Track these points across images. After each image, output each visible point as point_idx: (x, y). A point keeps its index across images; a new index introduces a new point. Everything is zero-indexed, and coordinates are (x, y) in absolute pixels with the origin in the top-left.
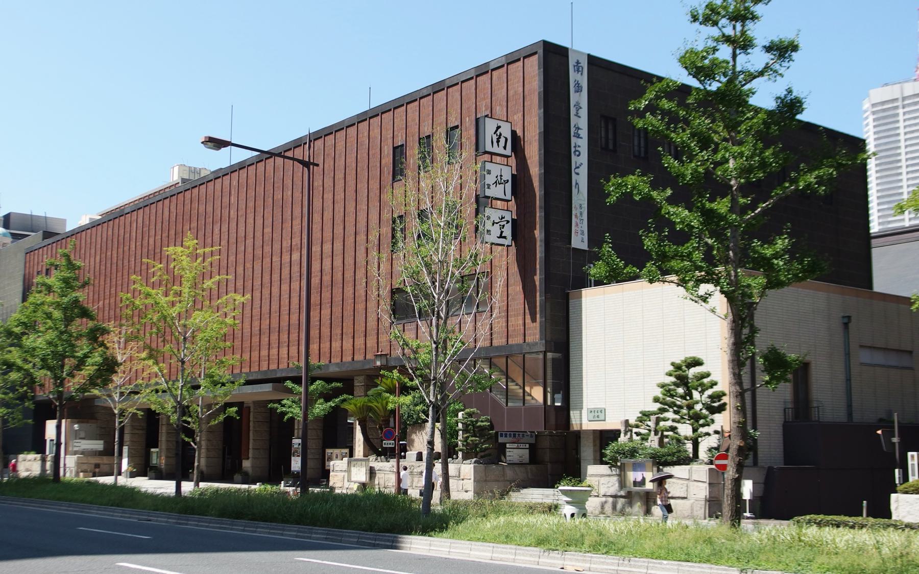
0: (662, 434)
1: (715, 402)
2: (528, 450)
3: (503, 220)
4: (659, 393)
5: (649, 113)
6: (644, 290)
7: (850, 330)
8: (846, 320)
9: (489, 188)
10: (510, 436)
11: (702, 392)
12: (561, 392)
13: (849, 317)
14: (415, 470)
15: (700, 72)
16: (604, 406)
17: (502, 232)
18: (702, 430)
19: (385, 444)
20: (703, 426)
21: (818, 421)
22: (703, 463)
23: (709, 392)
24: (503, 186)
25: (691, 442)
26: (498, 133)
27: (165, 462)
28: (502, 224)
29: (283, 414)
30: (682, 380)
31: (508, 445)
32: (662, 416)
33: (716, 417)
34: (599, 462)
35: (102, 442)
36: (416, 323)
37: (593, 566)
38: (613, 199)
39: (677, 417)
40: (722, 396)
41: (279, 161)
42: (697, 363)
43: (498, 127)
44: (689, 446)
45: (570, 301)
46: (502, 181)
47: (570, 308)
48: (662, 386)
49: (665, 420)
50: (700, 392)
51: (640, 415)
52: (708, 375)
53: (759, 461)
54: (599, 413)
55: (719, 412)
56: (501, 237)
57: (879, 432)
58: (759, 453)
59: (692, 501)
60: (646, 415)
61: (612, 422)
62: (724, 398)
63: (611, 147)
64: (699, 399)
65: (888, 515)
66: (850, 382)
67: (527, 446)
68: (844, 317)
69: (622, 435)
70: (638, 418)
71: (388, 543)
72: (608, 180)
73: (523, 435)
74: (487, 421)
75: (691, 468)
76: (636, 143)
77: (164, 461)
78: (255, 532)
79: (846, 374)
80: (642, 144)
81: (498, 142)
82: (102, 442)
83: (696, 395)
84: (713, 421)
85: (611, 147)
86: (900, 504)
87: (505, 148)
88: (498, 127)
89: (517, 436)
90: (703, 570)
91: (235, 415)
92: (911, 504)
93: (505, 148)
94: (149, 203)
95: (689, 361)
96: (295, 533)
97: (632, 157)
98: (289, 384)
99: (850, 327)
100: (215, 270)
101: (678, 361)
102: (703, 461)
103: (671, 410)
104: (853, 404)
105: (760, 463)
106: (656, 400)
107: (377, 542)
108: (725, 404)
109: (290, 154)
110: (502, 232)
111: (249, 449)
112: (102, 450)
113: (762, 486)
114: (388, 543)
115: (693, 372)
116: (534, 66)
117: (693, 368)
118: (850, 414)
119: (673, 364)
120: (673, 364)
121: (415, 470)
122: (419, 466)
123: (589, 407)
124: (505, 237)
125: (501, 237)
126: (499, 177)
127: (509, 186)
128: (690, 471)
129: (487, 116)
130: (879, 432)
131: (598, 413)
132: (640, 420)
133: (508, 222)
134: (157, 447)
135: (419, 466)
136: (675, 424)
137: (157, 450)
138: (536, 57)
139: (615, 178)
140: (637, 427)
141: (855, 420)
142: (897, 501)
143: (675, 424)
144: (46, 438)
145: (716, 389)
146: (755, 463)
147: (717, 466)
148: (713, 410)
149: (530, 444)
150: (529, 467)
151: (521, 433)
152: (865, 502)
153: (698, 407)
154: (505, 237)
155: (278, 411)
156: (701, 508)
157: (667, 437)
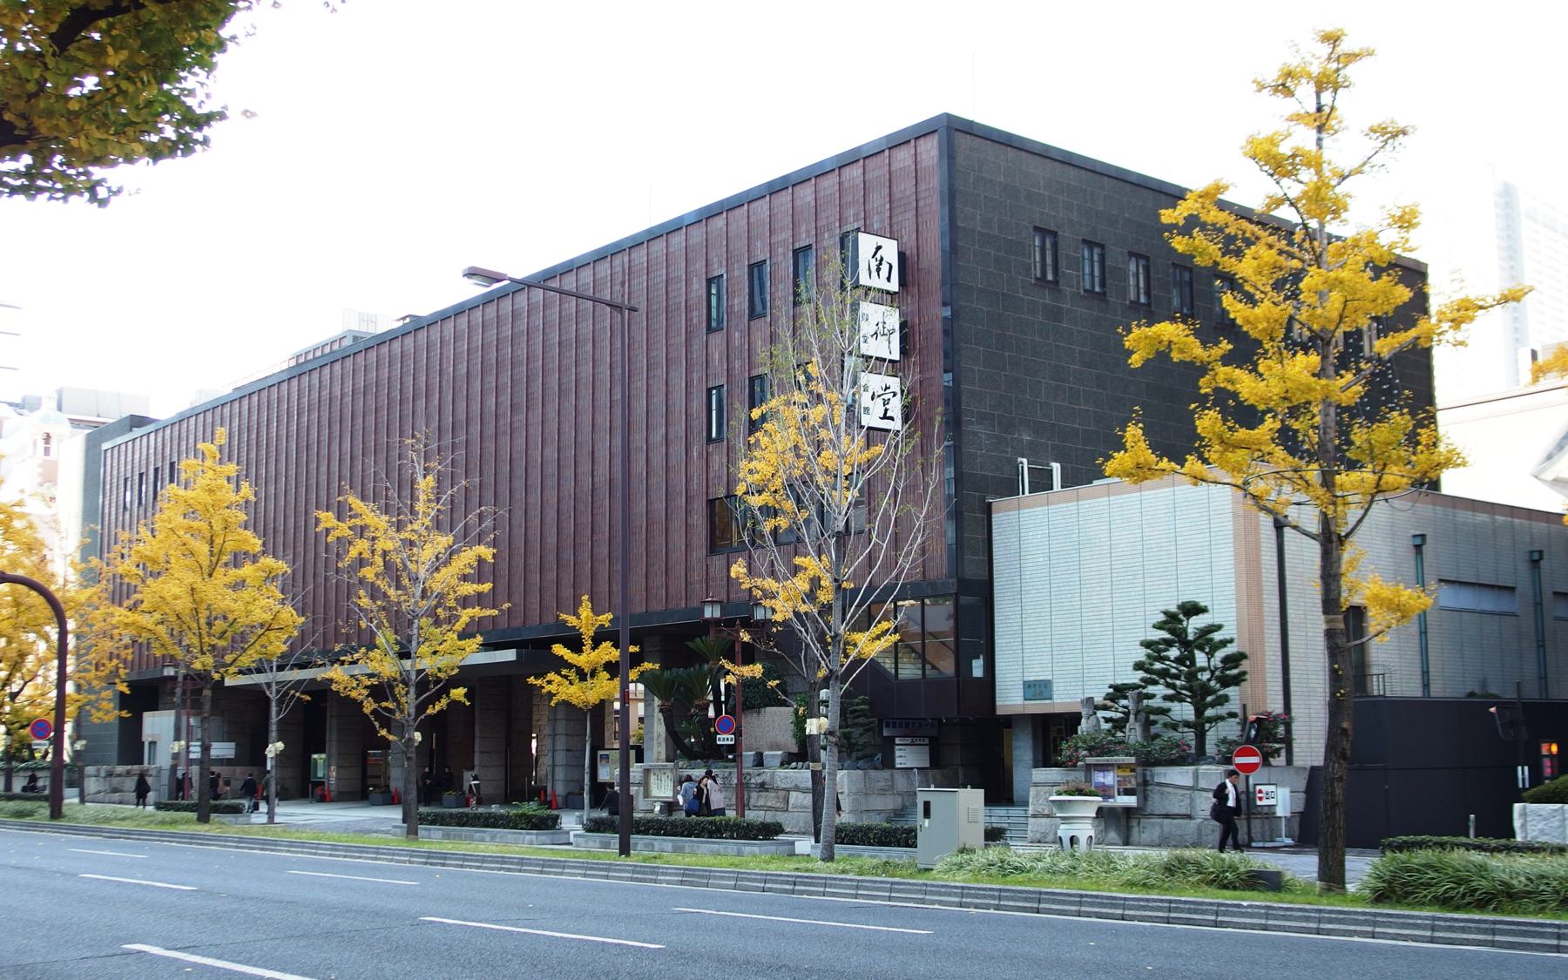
0: (1147, 718)
1: (1230, 669)
2: (927, 748)
3: (888, 391)
4: (1141, 654)
5: (1198, 229)
6: (1111, 498)
7: (1424, 556)
8: (1418, 541)
9: (865, 342)
10: (901, 726)
11: (1210, 655)
12: (981, 657)
13: (1423, 536)
14: (753, 781)
15: (1279, 166)
16: (1050, 678)
17: (886, 410)
18: (1209, 712)
19: (719, 739)
20: (1212, 705)
21: (1384, 696)
22: (1212, 761)
23: (1220, 654)
24: (886, 338)
25: (46, 804)
26: (878, 256)
27: (337, 774)
28: (886, 397)
29: (551, 695)
30: (1179, 637)
31: (897, 741)
32: (1145, 691)
33: (1231, 691)
34: (1041, 764)
35: (233, 745)
36: (747, 552)
37: (1127, 912)
38: (1136, 361)
39: (1171, 692)
40: (1241, 660)
41: (538, 294)
42: (1193, 609)
43: (879, 248)
44: (1190, 736)
45: (993, 516)
46: (886, 331)
47: (994, 527)
48: (1147, 644)
49: (1152, 696)
50: (1207, 654)
51: (1111, 690)
52: (1219, 627)
53: (1295, 758)
54: (1043, 689)
55: (1237, 684)
56: (885, 417)
57: (1493, 710)
58: (1294, 745)
59: (1199, 821)
60: (1119, 691)
61: (1064, 699)
62: (1244, 662)
63: (1050, 277)
64: (1206, 664)
65: (1511, 833)
66: (1426, 636)
67: (927, 741)
68: (1415, 536)
69: (1083, 721)
70: (1108, 694)
71: (787, 887)
72: (1129, 331)
73: (920, 724)
74: (863, 702)
75: (1197, 770)
76: (1087, 270)
77: (334, 774)
78: (562, 874)
79: (1420, 624)
80: (1097, 273)
81: (878, 270)
82: (233, 745)
83: (1201, 659)
84: (1226, 699)
85: (1050, 277)
86: (1529, 819)
87: (889, 279)
88: (879, 248)
89: (911, 726)
90: (1307, 914)
91: (463, 699)
92: (1545, 819)
93: (889, 279)
94: (307, 370)
95: (1188, 606)
96: (630, 875)
97: (1082, 292)
98: (559, 649)
99: (1424, 552)
100: (460, 471)
101: (1173, 609)
102: (1213, 758)
103: (1162, 681)
104: (1431, 669)
105: (1297, 761)
106: (1139, 666)
107: (768, 885)
108: (1244, 673)
109: (555, 284)
110: (886, 410)
111: (474, 752)
112: (233, 757)
113: (1303, 796)
114: (787, 887)
115: (1194, 624)
116: (930, 149)
117: (1194, 617)
118: (1426, 686)
119: (1166, 613)
120: (1166, 613)
121: (753, 781)
122: (759, 775)
123: (1026, 679)
124: (892, 418)
125: (885, 417)
126: (881, 325)
127: (896, 338)
128: (1196, 776)
129: (858, 230)
130: (1493, 710)
131: (1037, 689)
132: (1109, 697)
133: (895, 395)
134: (322, 751)
135: (759, 775)
136: (1167, 704)
137: (323, 756)
138: (936, 136)
139: (1139, 326)
140: (1105, 708)
141: (1432, 694)
142: (1524, 814)
143: (1167, 704)
144: (143, 739)
145: (1230, 650)
146: (1289, 761)
147: (1237, 765)
148: (1226, 682)
149: (931, 738)
150: (931, 773)
151: (917, 722)
152: (1472, 816)
153: (1205, 676)
154: (892, 418)
155: (544, 691)
156: (1213, 831)
157: (1154, 722)
